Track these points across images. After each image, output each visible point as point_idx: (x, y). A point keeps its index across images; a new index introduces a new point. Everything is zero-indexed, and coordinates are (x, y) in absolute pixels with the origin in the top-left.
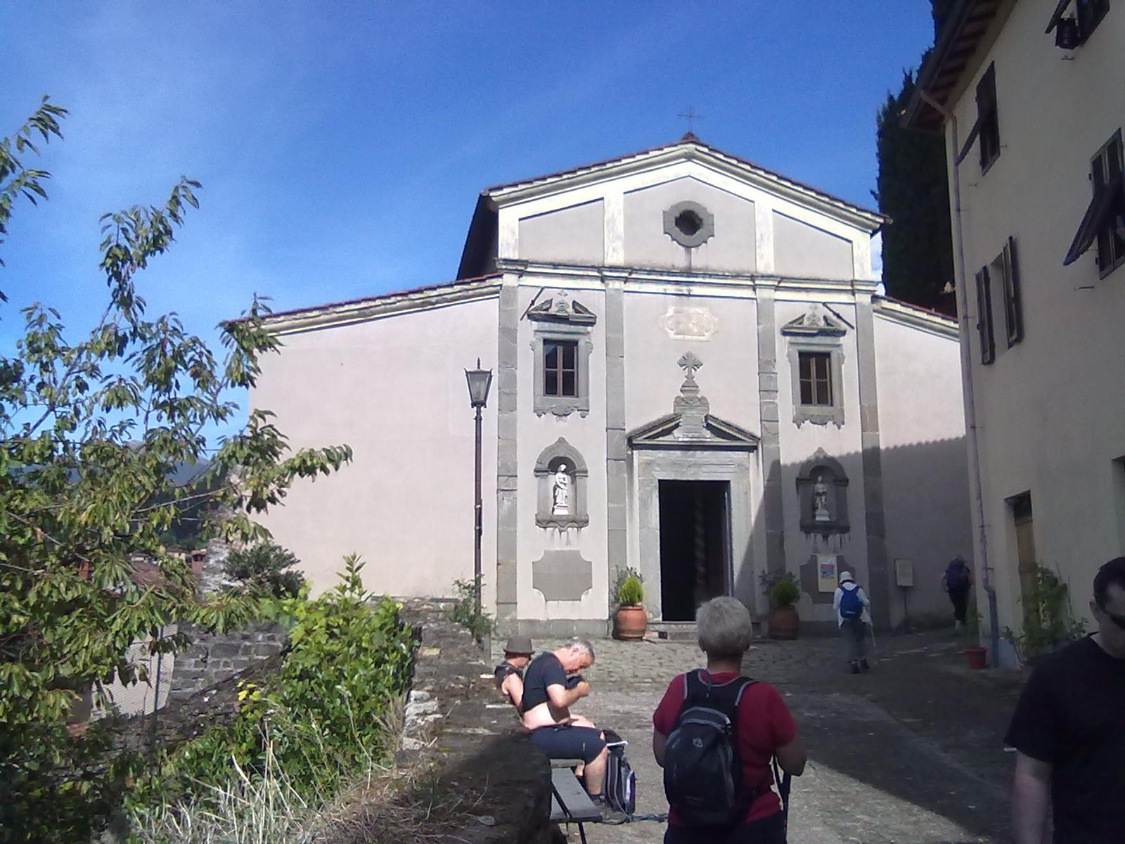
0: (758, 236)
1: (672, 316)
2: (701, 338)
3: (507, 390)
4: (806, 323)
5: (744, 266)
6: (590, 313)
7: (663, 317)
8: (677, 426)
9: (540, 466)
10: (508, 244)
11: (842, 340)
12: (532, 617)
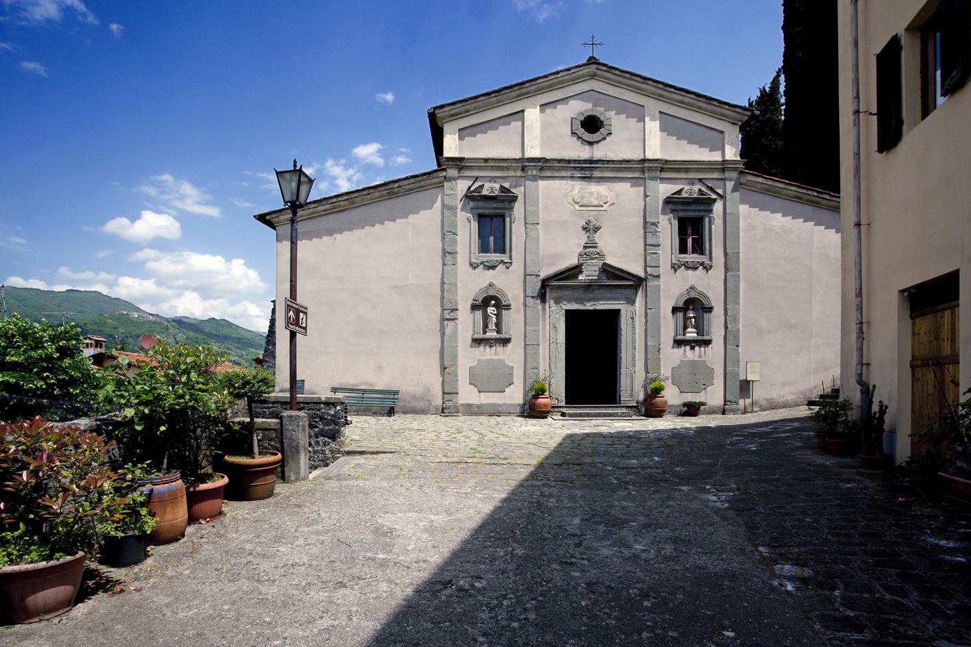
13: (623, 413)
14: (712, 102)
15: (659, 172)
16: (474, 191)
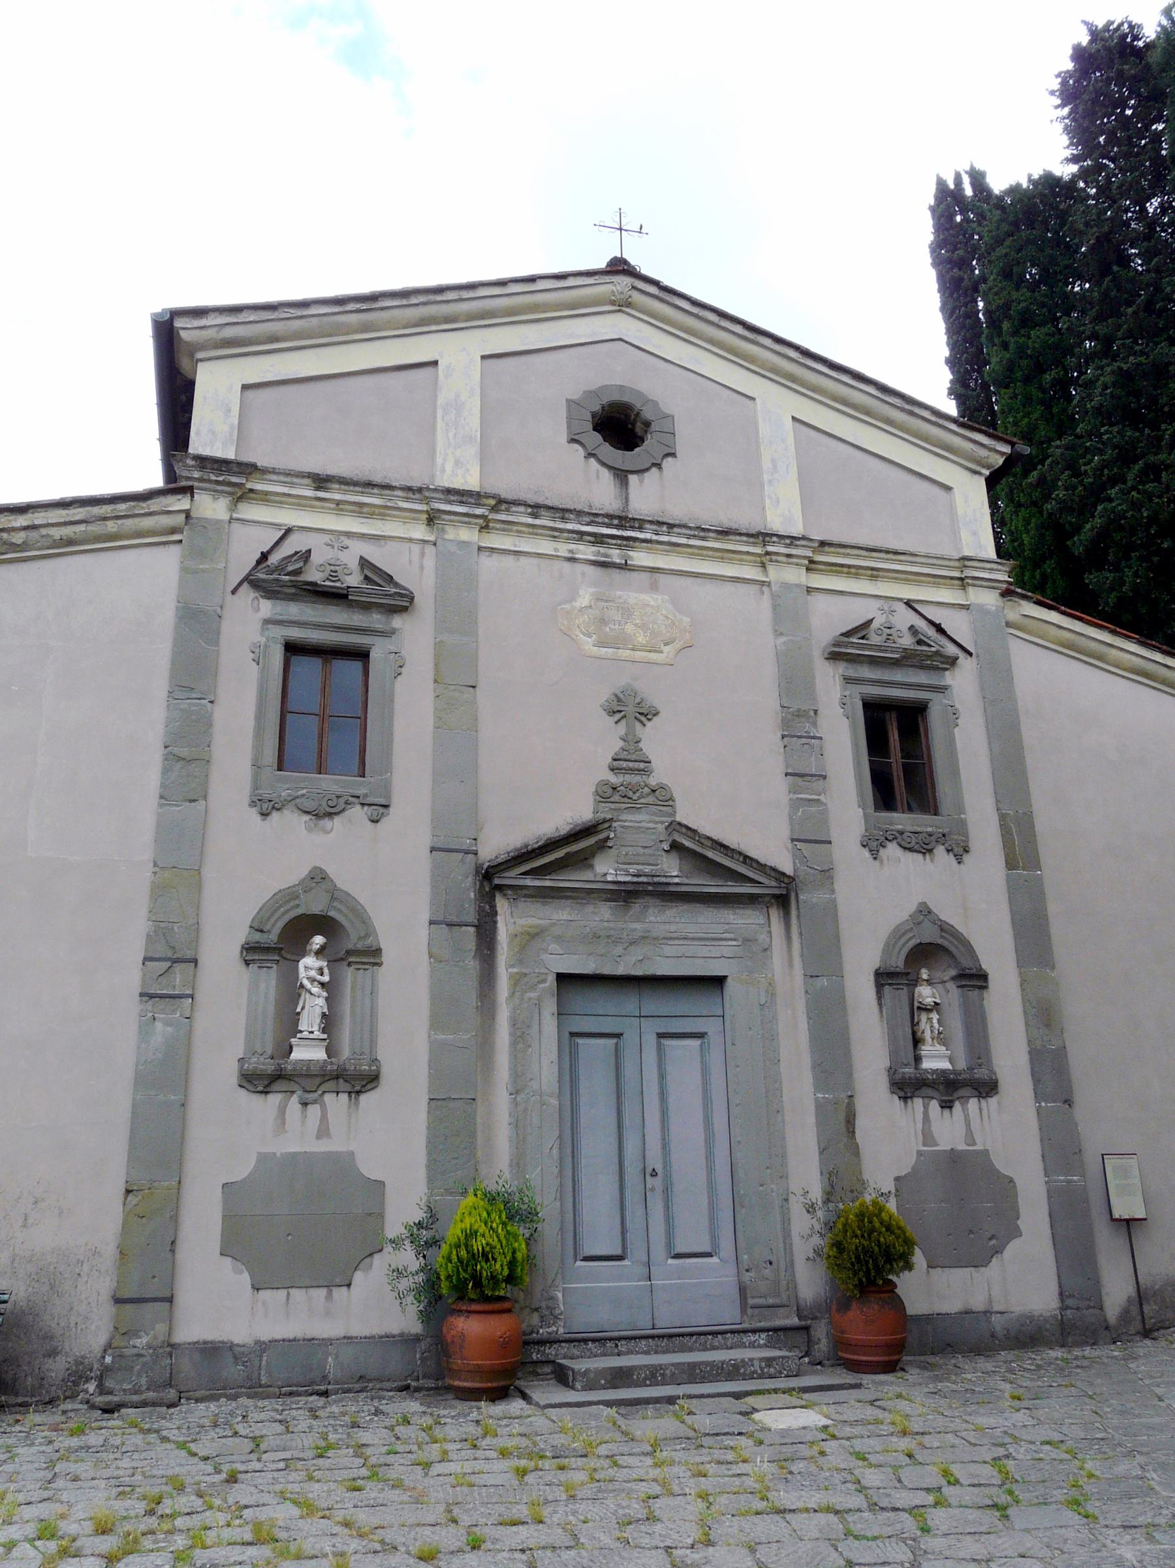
0: (766, 464)
2: (653, 656)
3: (184, 752)
4: (875, 639)
5: (745, 519)
6: (396, 585)
7: (567, 606)
8: (602, 846)
9: (258, 937)
10: (213, 433)
11: (949, 678)
12: (209, 1337)
13: (769, 1361)
14: (917, 410)
15: (804, 570)
16: (279, 568)
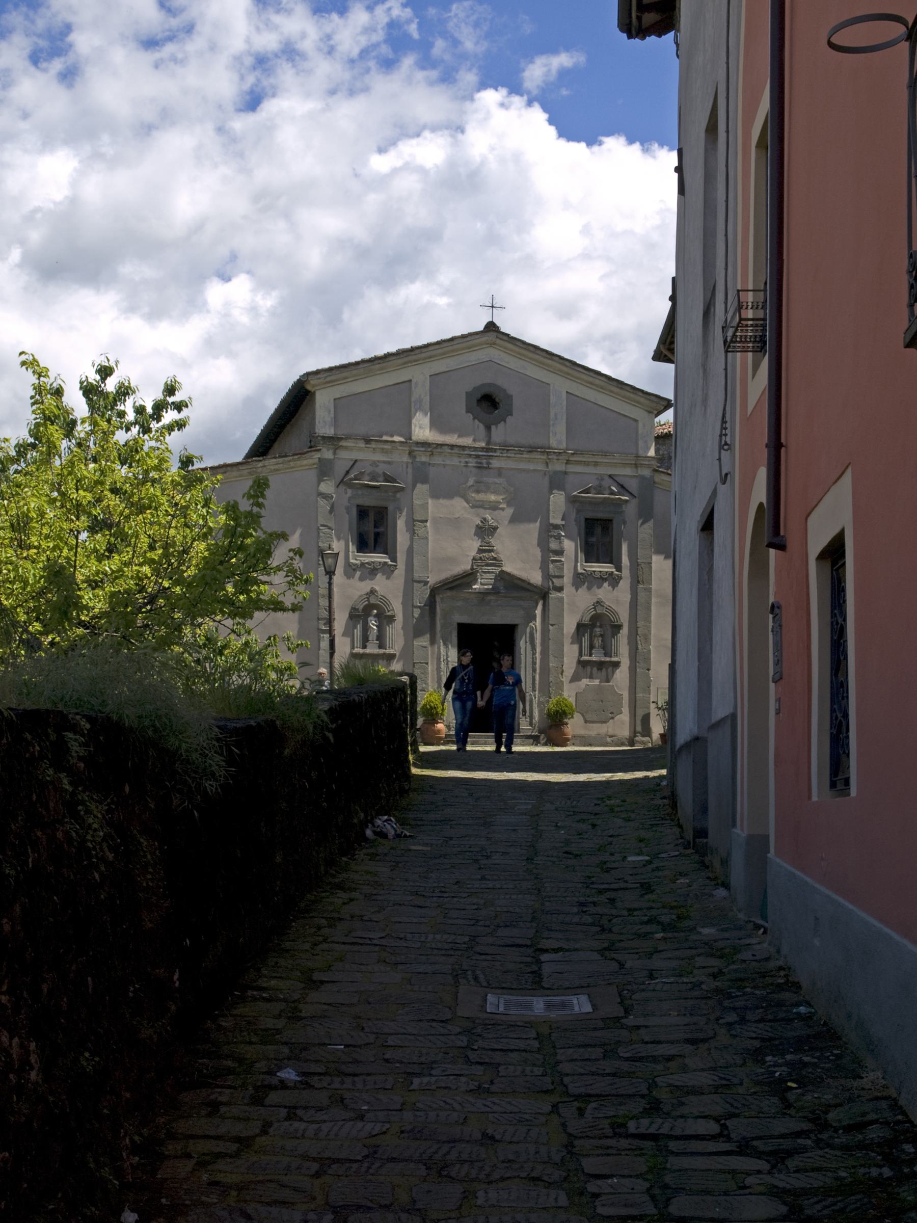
1: (473, 486)
10: (324, 422)
